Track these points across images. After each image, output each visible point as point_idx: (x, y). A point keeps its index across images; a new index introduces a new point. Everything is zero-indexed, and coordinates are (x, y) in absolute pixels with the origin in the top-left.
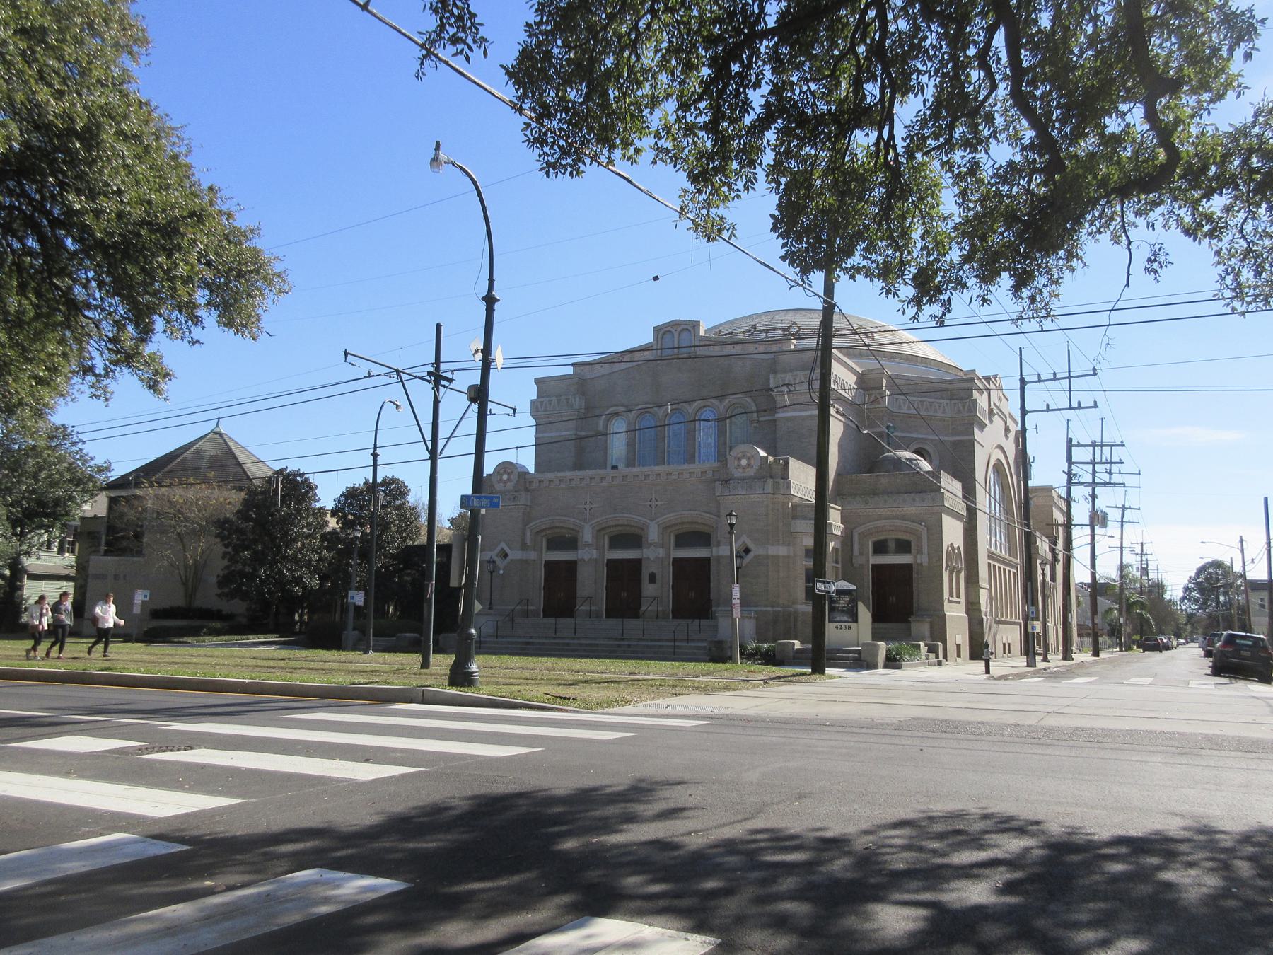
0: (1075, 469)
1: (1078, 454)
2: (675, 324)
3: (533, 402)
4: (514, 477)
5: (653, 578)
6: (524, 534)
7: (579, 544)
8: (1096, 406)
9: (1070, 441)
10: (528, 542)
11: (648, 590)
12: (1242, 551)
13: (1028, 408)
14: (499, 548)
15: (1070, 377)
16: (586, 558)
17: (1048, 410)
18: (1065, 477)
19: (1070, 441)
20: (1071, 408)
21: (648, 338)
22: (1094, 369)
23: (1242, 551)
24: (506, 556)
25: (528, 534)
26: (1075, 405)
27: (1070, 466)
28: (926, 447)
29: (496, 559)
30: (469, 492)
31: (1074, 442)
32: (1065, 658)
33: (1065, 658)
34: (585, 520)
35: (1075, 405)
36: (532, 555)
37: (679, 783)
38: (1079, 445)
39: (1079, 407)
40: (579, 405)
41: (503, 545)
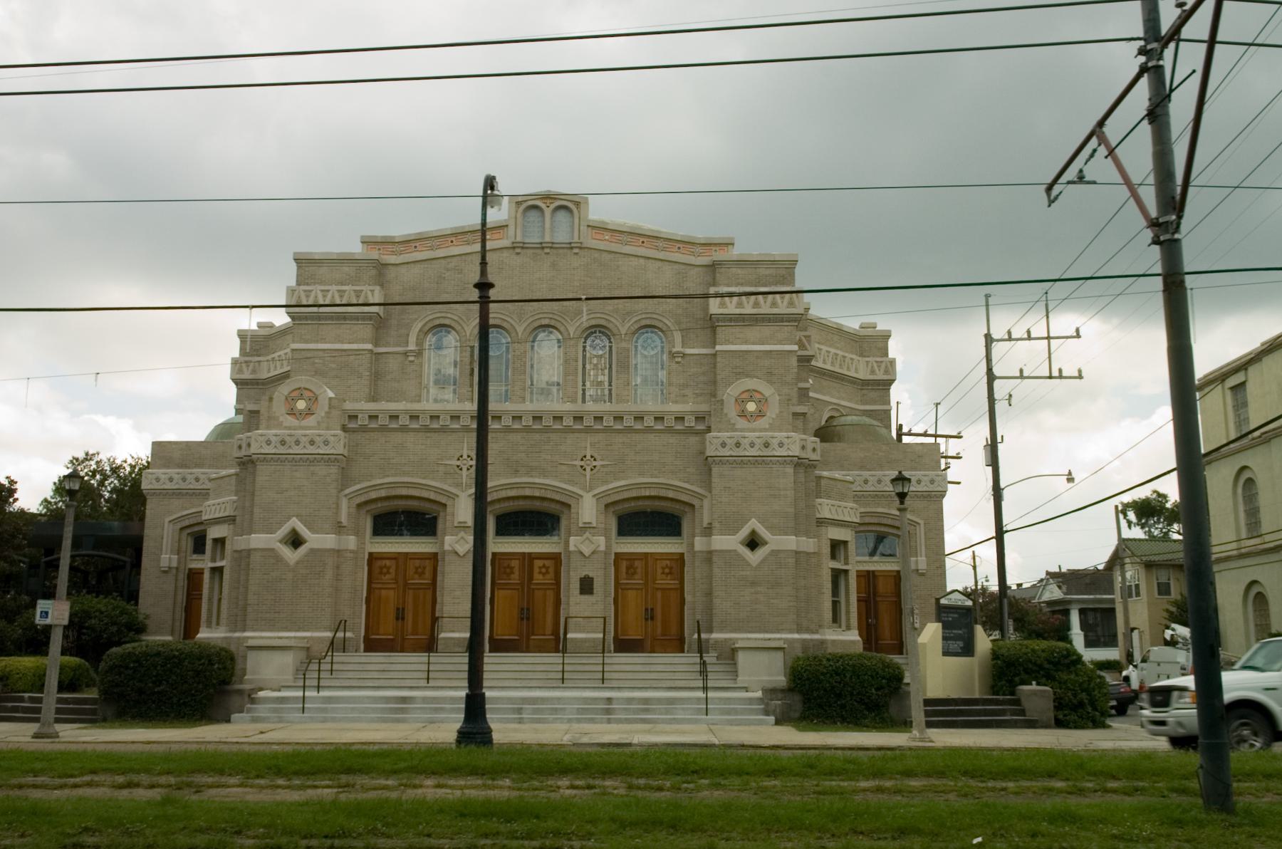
2: (548, 197)
5: (587, 586)
6: (338, 506)
11: (576, 604)
12: (974, 568)
13: (996, 371)
15: (1048, 338)
16: (587, 552)
17: (1022, 376)
20: (1050, 377)
22: (1080, 371)
23: (974, 568)
25: (344, 504)
26: (1055, 373)
31: (905, 430)
35: (1055, 373)
36: (351, 542)
39: (1061, 377)
41: (296, 523)
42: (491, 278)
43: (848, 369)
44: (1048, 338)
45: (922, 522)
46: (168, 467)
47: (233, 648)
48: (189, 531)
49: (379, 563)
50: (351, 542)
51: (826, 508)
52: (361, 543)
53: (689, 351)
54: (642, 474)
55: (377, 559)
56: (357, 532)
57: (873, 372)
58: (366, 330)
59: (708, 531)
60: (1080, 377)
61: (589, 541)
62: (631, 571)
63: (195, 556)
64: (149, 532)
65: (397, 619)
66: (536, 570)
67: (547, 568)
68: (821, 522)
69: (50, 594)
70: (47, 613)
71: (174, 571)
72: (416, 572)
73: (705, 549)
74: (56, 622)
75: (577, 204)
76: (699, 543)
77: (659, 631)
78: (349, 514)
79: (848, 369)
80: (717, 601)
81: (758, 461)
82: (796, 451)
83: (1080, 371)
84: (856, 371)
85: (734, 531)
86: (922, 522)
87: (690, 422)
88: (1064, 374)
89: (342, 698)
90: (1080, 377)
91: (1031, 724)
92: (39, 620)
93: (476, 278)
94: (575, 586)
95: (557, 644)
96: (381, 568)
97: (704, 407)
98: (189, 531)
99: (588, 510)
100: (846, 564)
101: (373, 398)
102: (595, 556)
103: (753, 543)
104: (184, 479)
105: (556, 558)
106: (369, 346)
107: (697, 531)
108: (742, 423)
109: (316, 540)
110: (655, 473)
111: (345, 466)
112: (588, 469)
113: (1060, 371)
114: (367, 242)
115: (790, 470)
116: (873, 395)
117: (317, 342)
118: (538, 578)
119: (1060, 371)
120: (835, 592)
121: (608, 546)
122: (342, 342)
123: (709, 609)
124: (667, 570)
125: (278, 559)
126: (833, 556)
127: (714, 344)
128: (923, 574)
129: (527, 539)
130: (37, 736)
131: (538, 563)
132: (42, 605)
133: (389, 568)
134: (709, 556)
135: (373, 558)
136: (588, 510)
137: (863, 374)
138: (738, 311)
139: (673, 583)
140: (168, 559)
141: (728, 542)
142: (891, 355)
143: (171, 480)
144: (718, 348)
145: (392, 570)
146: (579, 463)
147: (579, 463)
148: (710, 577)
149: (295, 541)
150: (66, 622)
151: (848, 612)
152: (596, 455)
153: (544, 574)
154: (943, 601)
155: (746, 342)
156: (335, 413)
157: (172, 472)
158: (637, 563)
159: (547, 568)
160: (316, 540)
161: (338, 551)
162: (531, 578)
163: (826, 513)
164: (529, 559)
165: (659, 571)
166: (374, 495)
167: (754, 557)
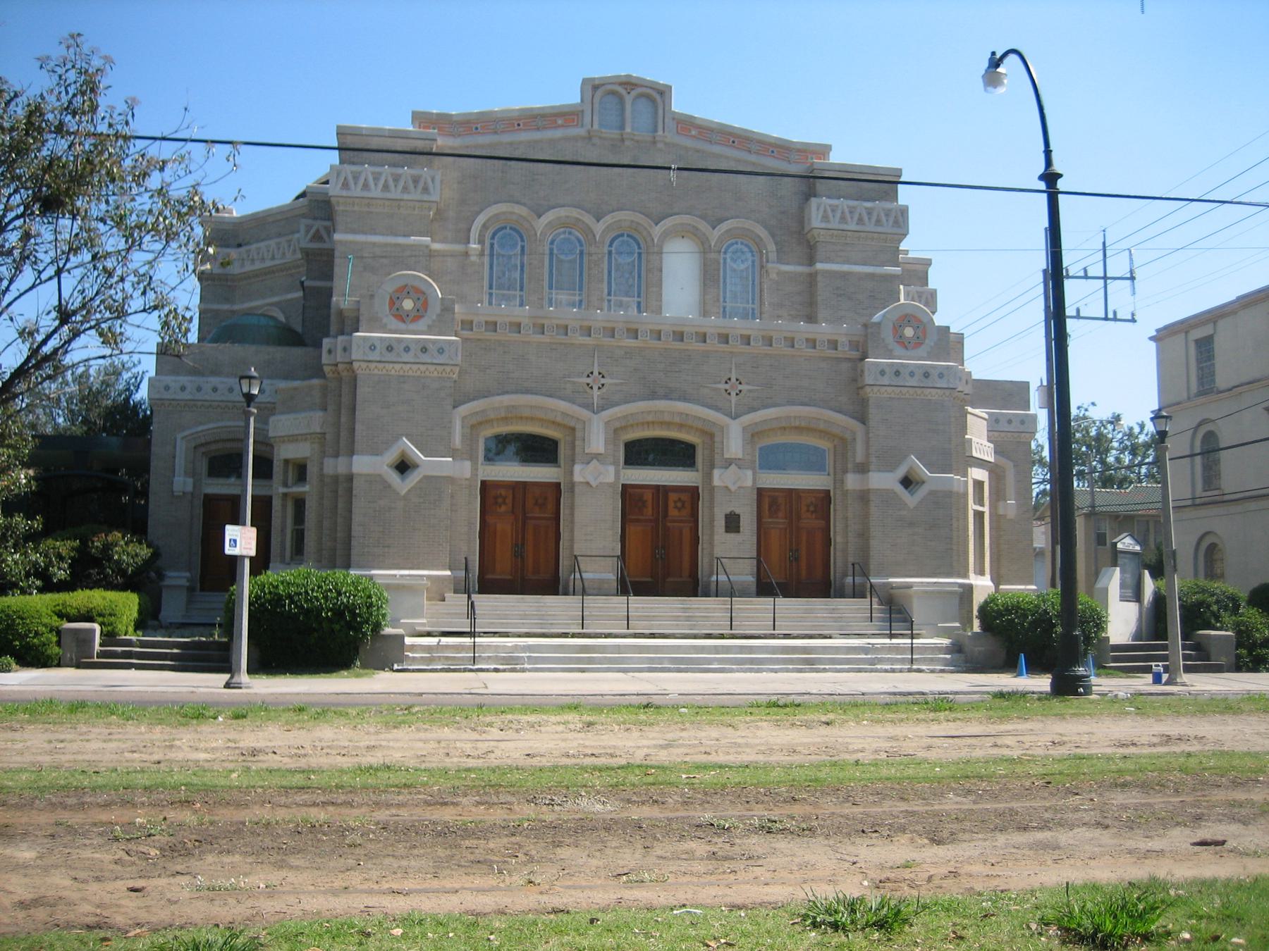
5: (732, 523)
20: (1106, 319)
21: (570, 96)
34: (588, 406)
35: (1111, 315)
39: (1115, 319)
42: (1057, 167)
46: (178, 374)
48: (203, 449)
52: (475, 469)
56: (472, 458)
59: (863, 469)
60: (1133, 320)
63: (210, 481)
64: (158, 450)
66: (671, 505)
67: (683, 503)
69: (237, 520)
70: (235, 541)
72: (536, 503)
73: (858, 488)
74: (245, 553)
75: (662, 93)
76: (852, 481)
77: (804, 573)
80: (873, 543)
85: (891, 468)
88: (1082, 314)
89: (751, 647)
90: (1133, 320)
91: (1218, 669)
92: (229, 551)
93: (1041, 169)
94: (720, 523)
95: (692, 586)
96: (496, 498)
98: (203, 449)
99: (597, 441)
103: (908, 482)
104: (199, 389)
105: (693, 492)
107: (850, 466)
109: (430, 463)
113: (1115, 313)
114: (418, 117)
117: (364, 233)
118: (673, 513)
119: (1115, 313)
121: (708, 476)
122: (396, 235)
123: (865, 550)
124: (812, 509)
125: (387, 486)
127: (811, 261)
130: (228, 686)
131: (673, 497)
132: (231, 531)
133: (504, 499)
134: (864, 497)
135: (761, 492)
136: (597, 441)
139: (822, 523)
140: (182, 483)
141: (884, 481)
142: (931, 285)
143: (183, 389)
144: (819, 266)
145: (509, 501)
147: (723, 386)
148: (866, 516)
150: (253, 553)
152: (741, 378)
153: (679, 509)
155: (848, 262)
157: (184, 380)
159: (683, 503)
160: (430, 463)
162: (666, 515)
164: (661, 492)
165: (804, 509)
167: (911, 500)
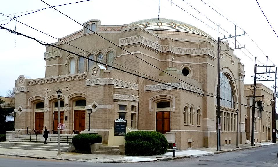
0: (257, 76)
1: (259, 70)
3: (45, 53)
4: (24, 81)
6: (27, 103)
7: (45, 105)
8: (245, 47)
9: (256, 65)
10: (29, 105)
14: (19, 108)
15: (236, 36)
18: (253, 79)
19: (256, 65)
20: (235, 49)
22: (244, 45)
24: (96, 107)
27: (255, 75)
28: (188, 67)
29: (92, 108)
30: (15, 87)
31: (257, 66)
32: (252, 145)
33: (252, 145)
37: (199, 164)
38: (259, 67)
39: (239, 48)
40: (59, 52)
41: (95, 102)
43: (192, 53)
44: (236, 36)
45: (174, 97)
47: (100, 134)
48: (156, 101)
49: (37, 114)
50: (29, 110)
51: (116, 97)
53: (118, 56)
54: (76, 91)
55: (37, 113)
57: (201, 53)
58: (57, 61)
60: (245, 47)
61: (68, 109)
62: (77, 114)
65: (79, 126)
68: (114, 101)
71: (48, 112)
78: (30, 104)
79: (192, 53)
81: (95, 86)
82: (102, 83)
83: (244, 45)
84: (196, 53)
86: (174, 97)
87: (84, 77)
97: (86, 73)
98: (156, 101)
100: (135, 111)
101: (59, 74)
102: (68, 111)
106: (57, 64)
108: (93, 76)
110: (77, 90)
111: (27, 93)
112: (47, 92)
113: (239, 46)
115: (102, 88)
116: (202, 59)
119: (239, 46)
120: (132, 119)
126: (132, 110)
128: (174, 112)
129: (79, 107)
137: (198, 54)
138: (129, 44)
146: (65, 89)
147: (65, 89)
149: (95, 106)
151: (135, 124)
154: (116, 121)
156: (26, 82)
158: (78, 113)
161: (105, 109)
163: (115, 98)
166: (33, 100)
